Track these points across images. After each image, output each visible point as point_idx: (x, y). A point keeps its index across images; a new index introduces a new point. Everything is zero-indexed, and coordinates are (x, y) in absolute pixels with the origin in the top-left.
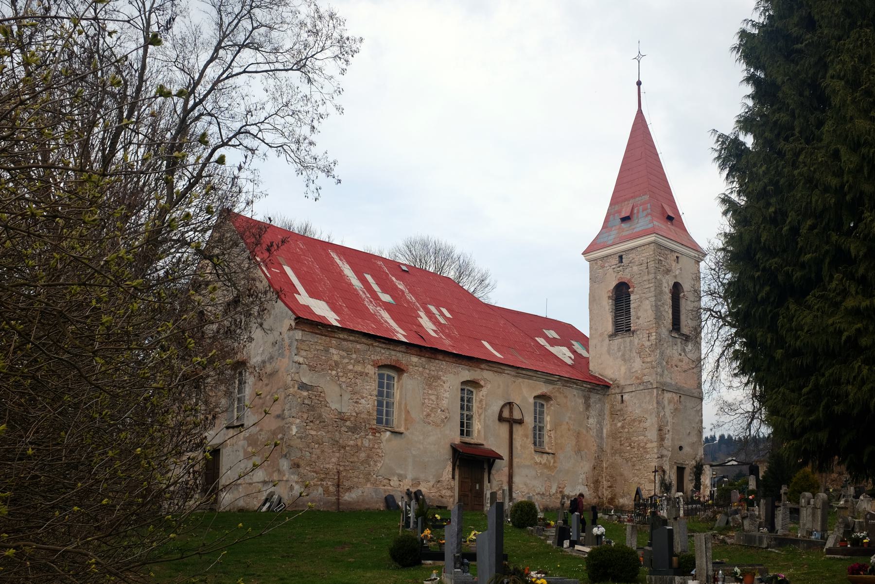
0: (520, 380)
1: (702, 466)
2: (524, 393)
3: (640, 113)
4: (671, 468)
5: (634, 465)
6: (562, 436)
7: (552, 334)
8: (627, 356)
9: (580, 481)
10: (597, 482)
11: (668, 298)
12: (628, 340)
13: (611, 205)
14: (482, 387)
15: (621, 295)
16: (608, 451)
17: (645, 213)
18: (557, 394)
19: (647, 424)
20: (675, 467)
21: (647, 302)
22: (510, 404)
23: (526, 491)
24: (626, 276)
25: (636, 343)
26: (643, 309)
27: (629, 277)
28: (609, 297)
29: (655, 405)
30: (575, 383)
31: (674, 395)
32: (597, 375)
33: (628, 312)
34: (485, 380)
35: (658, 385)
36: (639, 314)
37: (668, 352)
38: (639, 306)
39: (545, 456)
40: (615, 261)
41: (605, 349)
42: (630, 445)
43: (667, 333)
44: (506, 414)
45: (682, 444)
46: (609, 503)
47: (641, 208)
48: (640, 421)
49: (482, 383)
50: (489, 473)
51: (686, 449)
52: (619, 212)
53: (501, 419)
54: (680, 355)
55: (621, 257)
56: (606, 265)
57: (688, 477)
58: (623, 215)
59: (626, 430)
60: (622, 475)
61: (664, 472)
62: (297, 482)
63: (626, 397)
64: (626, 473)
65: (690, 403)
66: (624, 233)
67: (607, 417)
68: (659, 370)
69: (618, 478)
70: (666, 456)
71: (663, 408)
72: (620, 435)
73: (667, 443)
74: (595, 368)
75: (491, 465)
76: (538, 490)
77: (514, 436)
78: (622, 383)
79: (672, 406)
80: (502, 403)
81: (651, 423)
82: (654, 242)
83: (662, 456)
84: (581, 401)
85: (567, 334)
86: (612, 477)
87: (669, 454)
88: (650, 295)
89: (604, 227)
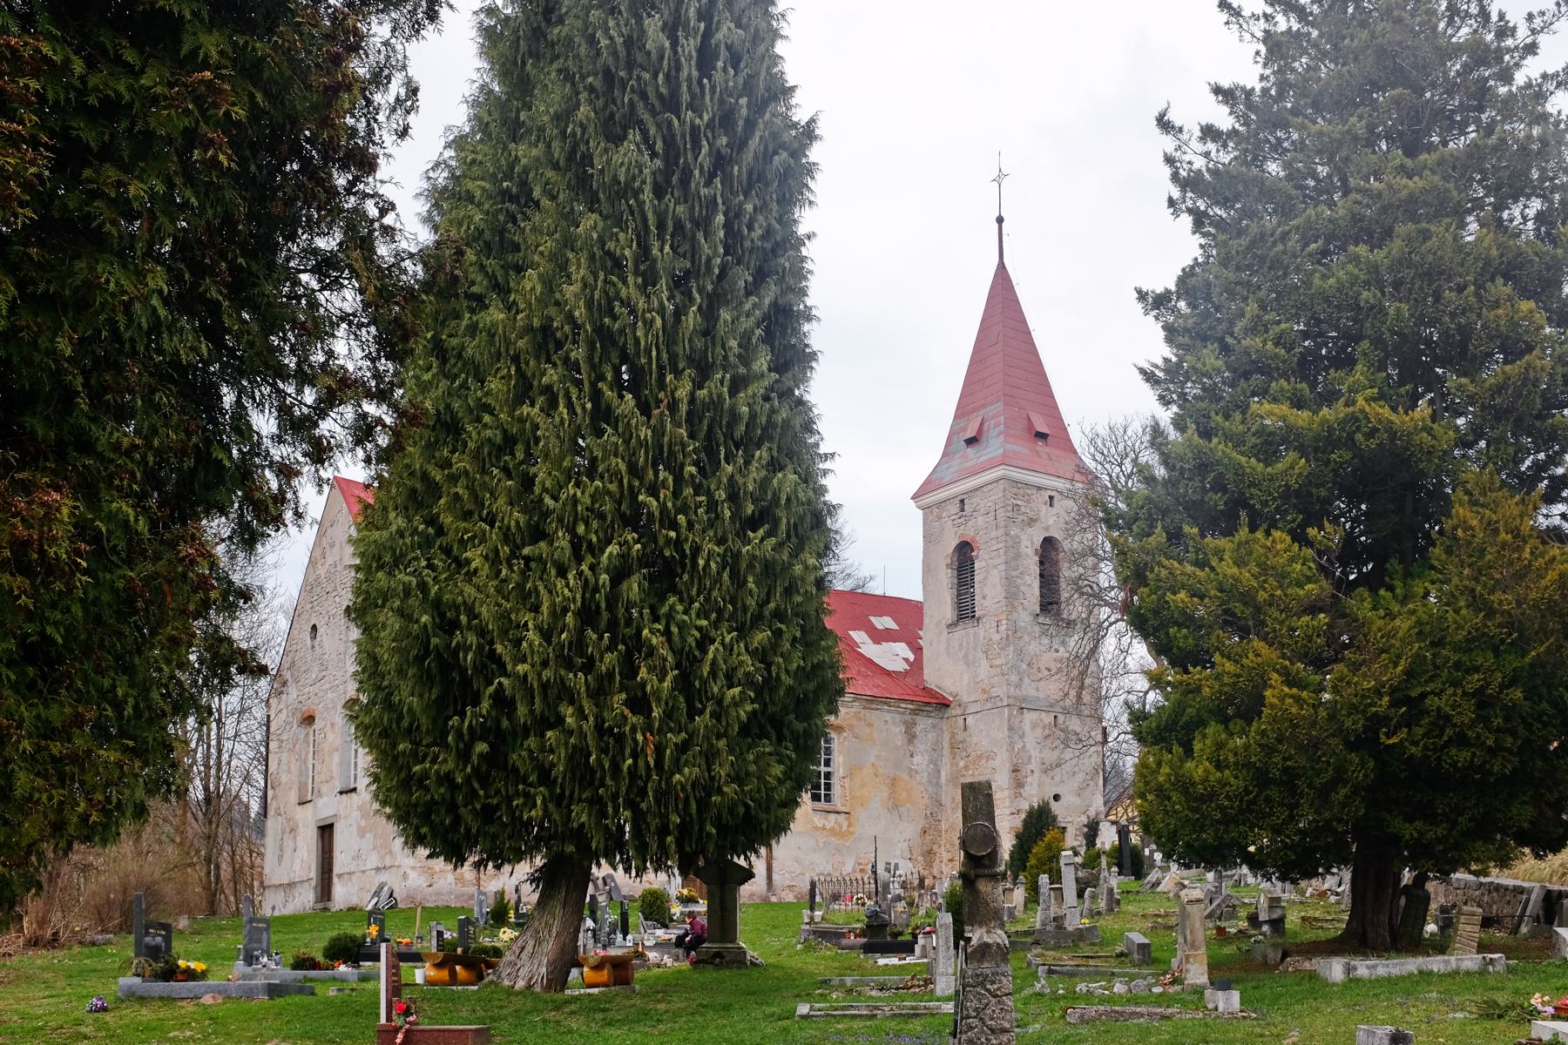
1: (1098, 823)
3: (1001, 266)
6: (863, 785)
7: (884, 622)
9: (898, 852)
11: (1032, 565)
12: (971, 631)
13: (956, 417)
15: (964, 556)
24: (969, 533)
35: (1011, 701)
39: (832, 817)
48: (988, 758)
55: (962, 501)
62: (413, 868)
66: (969, 464)
67: (946, 751)
71: (1022, 736)
74: (931, 678)
78: (965, 699)
79: (1039, 732)
84: (898, 730)
89: (945, 454)
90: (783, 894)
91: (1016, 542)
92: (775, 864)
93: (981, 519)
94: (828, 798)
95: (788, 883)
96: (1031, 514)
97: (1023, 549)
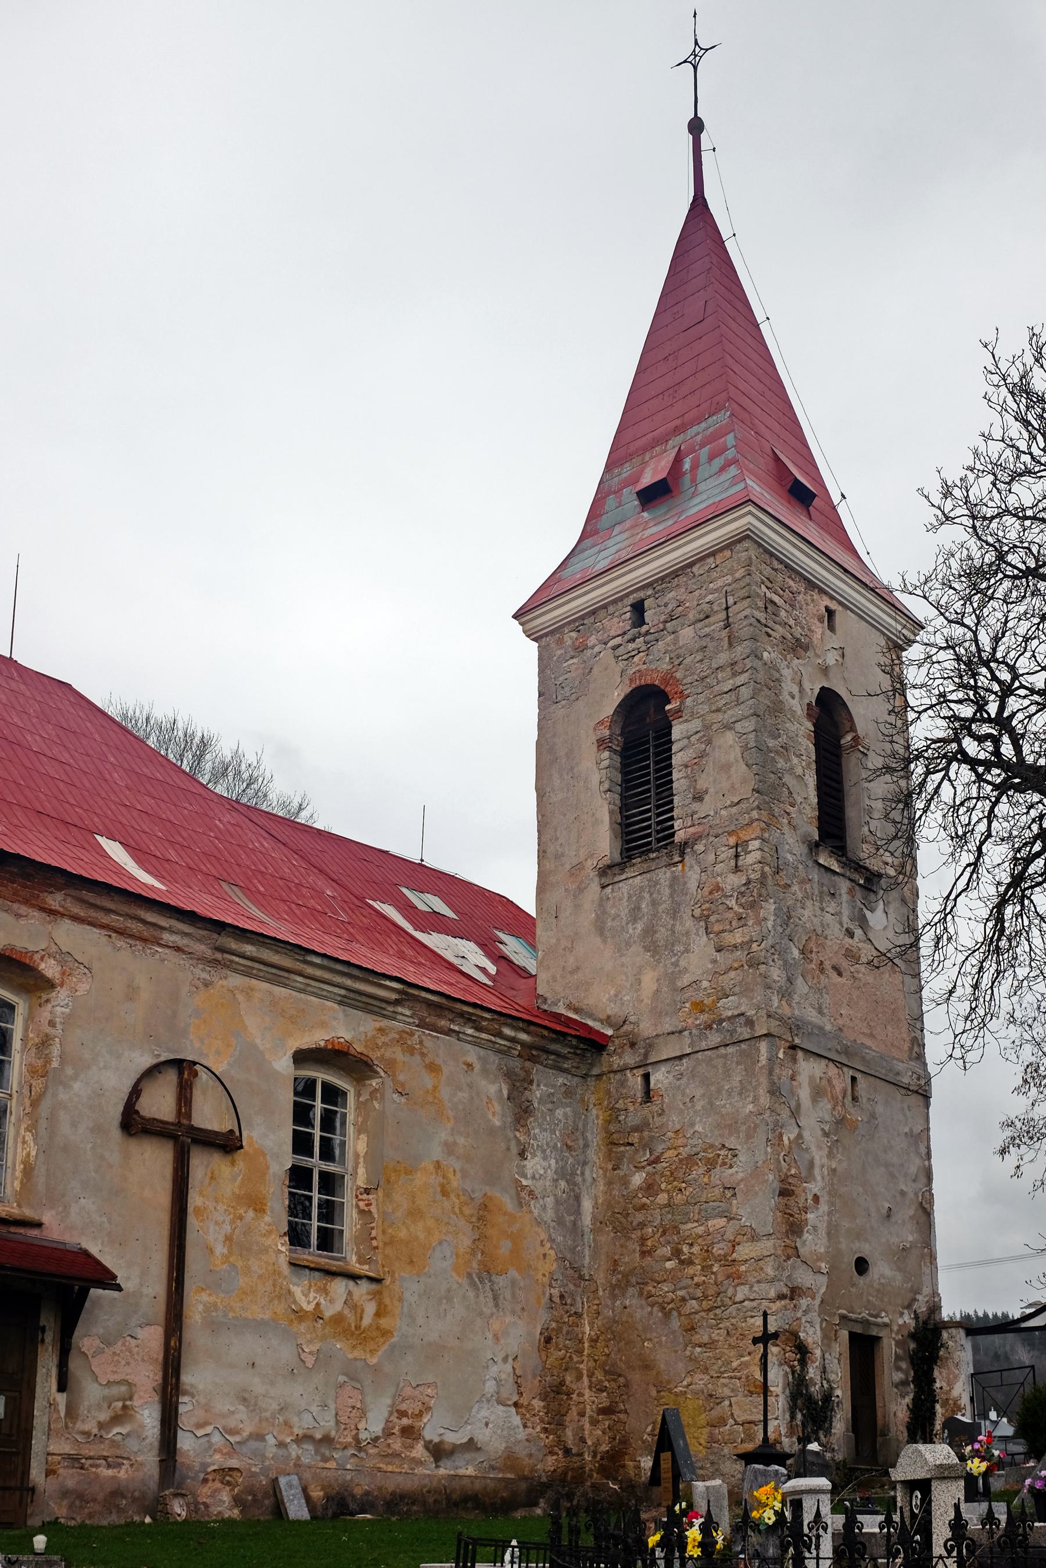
0: (236, 980)
2: (255, 1041)
3: (699, 206)
4: (829, 1337)
5: (691, 1329)
6: (415, 1213)
8: (662, 934)
9: (490, 1387)
10: (556, 1395)
11: (801, 731)
12: (664, 876)
13: (609, 466)
14: (49, 985)
15: (642, 734)
16: (601, 1278)
17: (718, 462)
18: (397, 1054)
19: (737, 1173)
20: (844, 1334)
21: (730, 737)
22: (184, 1070)
23: (248, 1429)
24: (654, 665)
25: (692, 885)
26: (712, 771)
27: (665, 666)
28: (601, 743)
29: (765, 1100)
30: (468, 1019)
31: (833, 1071)
32: (561, 1010)
33: (665, 784)
34: (63, 956)
35: (774, 1026)
36: (702, 783)
37: (808, 914)
38: (702, 755)
39: (339, 1287)
40: (619, 623)
41: (587, 918)
42: (677, 1253)
43: (801, 850)
44: (160, 1103)
45: (865, 1250)
46: (603, 1471)
47: (704, 452)
48: (711, 1164)
49: (49, 968)
50: (65, 1351)
51: (881, 1270)
52: (635, 479)
53: (133, 1123)
54: (850, 934)
55: (638, 608)
56: (592, 640)
57: (892, 1373)
58: (647, 479)
59: (662, 1198)
60: (647, 1366)
61: (802, 1350)
63: (659, 1078)
64: (662, 1358)
65: (887, 1107)
67: (594, 1155)
68: (776, 974)
69: (636, 1377)
70: (810, 1293)
71: (795, 1114)
72: (639, 1217)
73: (813, 1243)
75: (71, 1310)
76: (302, 1424)
77: (195, 1200)
78: (647, 1028)
80: (145, 1061)
81: (749, 1162)
82: (745, 536)
83: (794, 1293)
84: (495, 1088)
85: (481, 912)
86: (613, 1373)
87: (820, 1284)
88: (738, 712)
90: (204, 1493)
91: (774, 683)
92: (185, 1406)
93: (687, 634)
94: (328, 1241)
95: (217, 1461)
96: (798, 631)
97: (785, 697)
